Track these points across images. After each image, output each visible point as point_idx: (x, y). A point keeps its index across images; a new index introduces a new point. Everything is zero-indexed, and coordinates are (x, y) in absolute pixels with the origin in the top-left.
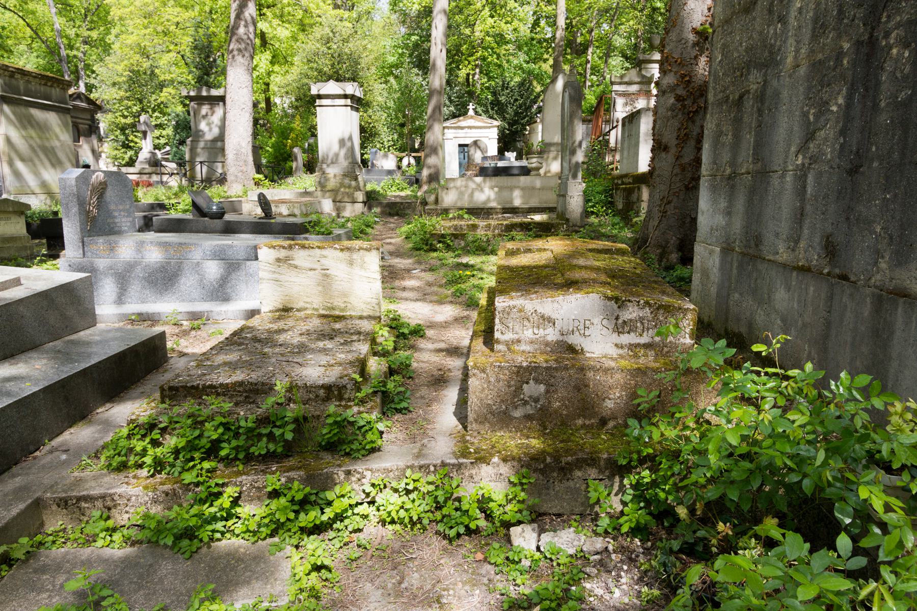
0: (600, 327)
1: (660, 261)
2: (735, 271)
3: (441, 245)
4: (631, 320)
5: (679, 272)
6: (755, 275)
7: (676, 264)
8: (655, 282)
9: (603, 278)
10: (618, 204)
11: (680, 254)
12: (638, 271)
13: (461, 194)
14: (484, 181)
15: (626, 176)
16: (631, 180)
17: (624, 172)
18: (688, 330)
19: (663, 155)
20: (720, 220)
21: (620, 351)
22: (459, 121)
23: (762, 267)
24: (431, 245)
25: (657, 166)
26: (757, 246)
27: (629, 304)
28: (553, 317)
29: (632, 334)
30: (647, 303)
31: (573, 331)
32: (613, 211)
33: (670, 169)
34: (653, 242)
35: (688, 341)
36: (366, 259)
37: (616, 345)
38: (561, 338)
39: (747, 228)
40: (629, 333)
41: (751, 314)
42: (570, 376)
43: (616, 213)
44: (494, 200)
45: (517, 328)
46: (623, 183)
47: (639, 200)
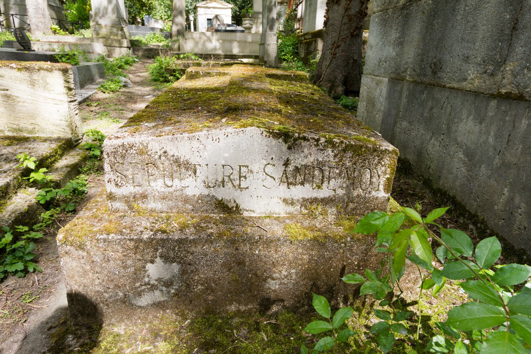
0: (262, 176)
1: (330, 92)
2: (404, 100)
3: (172, 77)
4: (306, 166)
5: (344, 101)
6: (430, 103)
7: (341, 95)
8: (336, 110)
9: (274, 103)
10: (301, 54)
11: (344, 87)
12: (316, 97)
13: (197, 43)
14: (212, 34)
15: (307, 34)
16: (310, 37)
17: (306, 32)
18: (383, 180)
19: (336, 7)
20: (390, 51)
21: (291, 209)
22: (207, 3)
23: (441, 95)
24: (166, 77)
25: (331, 17)
26: (434, 73)
27: (304, 143)
28: (194, 160)
29: (307, 186)
30: (330, 142)
31: (223, 182)
32: (298, 59)
33: (340, 19)
34: (325, 78)
35: (382, 194)
36: (48, 80)
37: (285, 201)
38: (206, 192)
39: (422, 57)
40: (302, 184)
41: (422, 143)
42: (216, 251)
43: (300, 60)
44: (219, 49)
45: (139, 178)
46: (305, 39)
47: (316, 49)
